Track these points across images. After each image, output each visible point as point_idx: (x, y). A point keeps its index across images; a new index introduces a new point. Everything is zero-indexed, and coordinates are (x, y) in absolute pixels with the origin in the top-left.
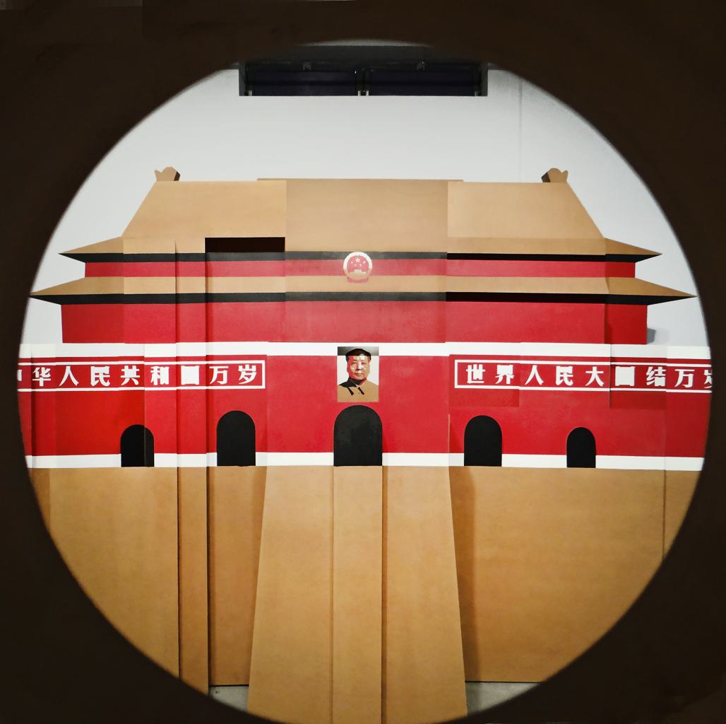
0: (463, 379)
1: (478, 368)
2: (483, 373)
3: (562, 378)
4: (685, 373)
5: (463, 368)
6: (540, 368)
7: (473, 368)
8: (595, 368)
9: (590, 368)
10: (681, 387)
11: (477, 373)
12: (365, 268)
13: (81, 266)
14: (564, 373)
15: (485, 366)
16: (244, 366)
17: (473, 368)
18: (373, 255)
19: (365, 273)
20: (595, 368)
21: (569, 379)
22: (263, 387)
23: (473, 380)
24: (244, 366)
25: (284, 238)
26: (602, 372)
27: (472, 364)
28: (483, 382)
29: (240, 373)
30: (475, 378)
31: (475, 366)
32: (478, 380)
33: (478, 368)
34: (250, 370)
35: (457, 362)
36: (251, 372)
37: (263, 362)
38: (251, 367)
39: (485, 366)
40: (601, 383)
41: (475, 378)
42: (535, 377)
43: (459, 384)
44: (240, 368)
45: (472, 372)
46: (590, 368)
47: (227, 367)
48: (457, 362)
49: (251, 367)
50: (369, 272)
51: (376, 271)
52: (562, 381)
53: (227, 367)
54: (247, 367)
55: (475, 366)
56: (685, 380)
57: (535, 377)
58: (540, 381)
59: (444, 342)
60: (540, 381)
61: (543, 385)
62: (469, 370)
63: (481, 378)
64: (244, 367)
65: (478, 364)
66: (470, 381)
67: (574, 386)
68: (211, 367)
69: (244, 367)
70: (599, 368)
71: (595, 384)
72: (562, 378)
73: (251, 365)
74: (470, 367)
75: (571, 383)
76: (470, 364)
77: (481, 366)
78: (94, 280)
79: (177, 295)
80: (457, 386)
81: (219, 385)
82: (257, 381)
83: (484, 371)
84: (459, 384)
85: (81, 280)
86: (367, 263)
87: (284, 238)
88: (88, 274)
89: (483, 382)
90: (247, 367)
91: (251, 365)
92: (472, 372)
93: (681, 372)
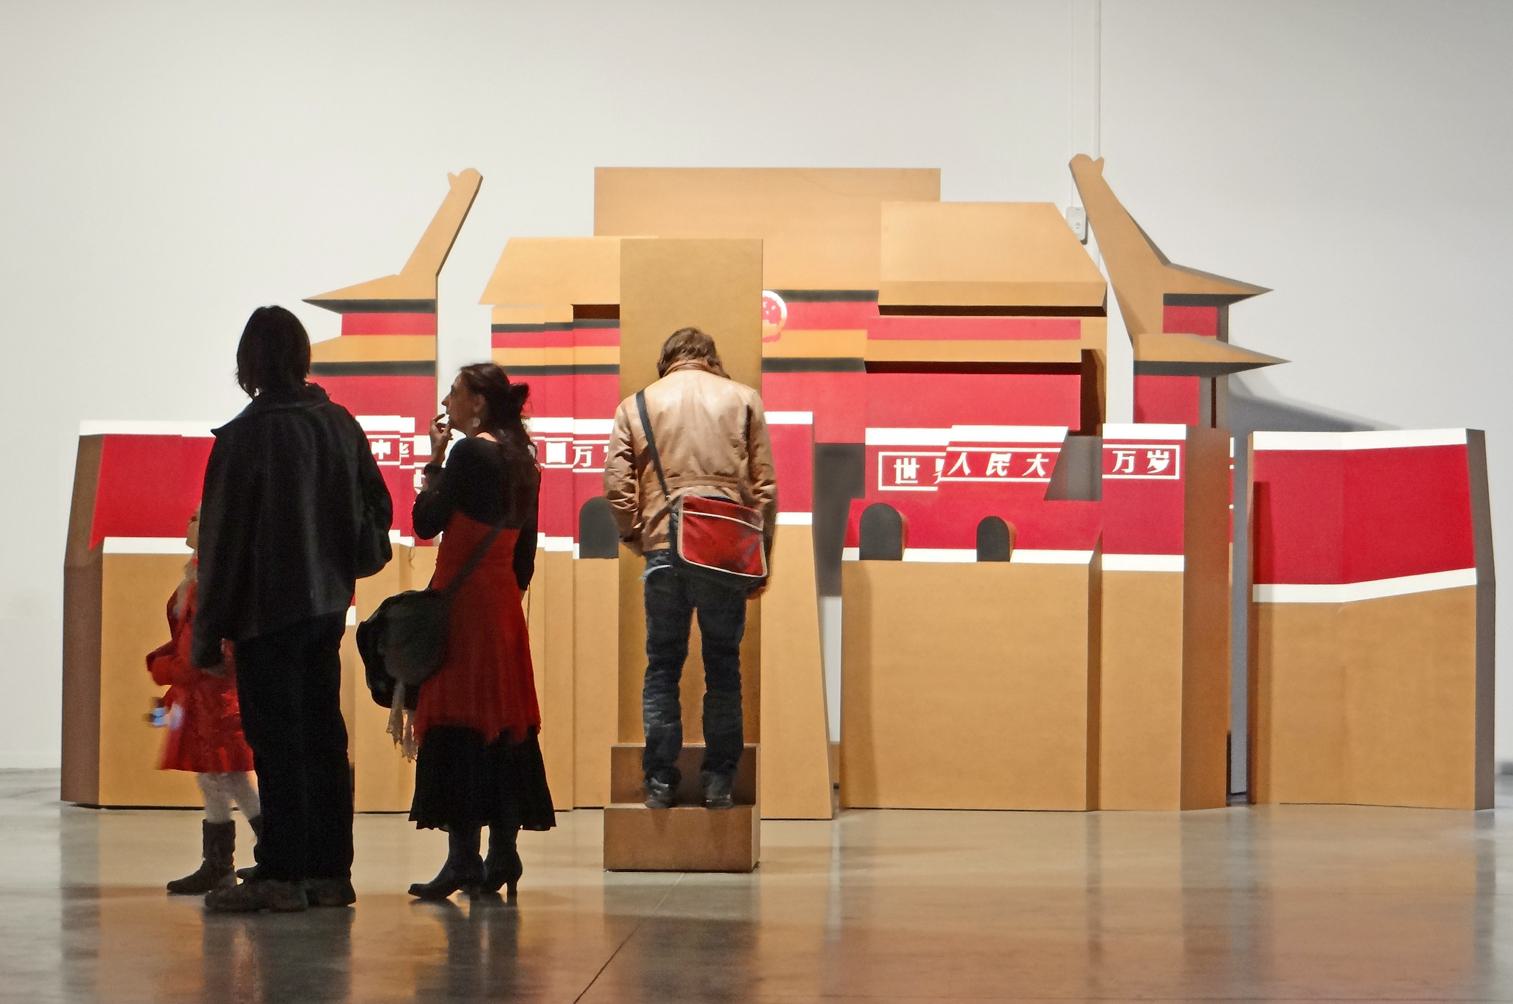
0: (890, 478)
1: (910, 463)
2: (917, 470)
3: (995, 467)
4: (1125, 455)
5: (890, 463)
6: (971, 457)
7: (902, 463)
8: (1039, 456)
9: (1033, 455)
10: (1120, 472)
11: (908, 469)
12: (775, 317)
13: (336, 319)
14: (999, 461)
15: (920, 460)
16: (1154, 451)
17: (902, 463)
18: (788, 295)
19: (775, 325)
20: (1039, 456)
21: (1004, 468)
22: (1177, 477)
23: (903, 479)
24: (1154, 451)
25: (1483, 432)
26: (1047, 460)
27: (902, 458)
28: (916, 482)
29: (1149, 460)
30: (906, 476)
31: (906, 460)
32: (909, 479)
33: (910, 463)
34: (1126, 458)
35: (881, 454)
36: (1162, 459)
37: (1177, 448)
38: (1162, 454)
39: (920, 460)
40: (1041, 472)
41: (906, 476)
42: (961, 467)
43: (884, 484)
44: (1150, 455)
45: (902, 470)
46: (1033, 455)
47: (1134, 452)
48: (881, 454)
49: (1162, 454)
50: (782, 324)
51: (794, 324)
52: (993, 471)
53: (1134, 452)
54: (1158, 453)
55: (906, 460)
56: (1125, 464)
57: (961, 467)
58: (967, 470)
59: (950, 427)
60: (967, 470)
61: (970, 475)
62: (898, 465)
63: (913, 476)
64: (1154, 453)
65: (910, 458)
66: (898, 480)
67: (1008, 476)
68: (1114, 452)
69: (1154, 453)
70: (1045, 455)
71: (1035, 474)
72: (995, 467)
73: (1163, 451)
74: (899, 461)
75: (1005, 473)
76: (1150, 450)
77: (914, 461)
78: (356, 340)
79: (574, 373)
80: (881, 488)
81: (1123, 473)
82: (1170, 470)
83: (918, 466)
84: (884, 484)
85: (335, 340)
86: (778, 309)
87: (1483, 432)
88: (347, 330)
89: (916, 482)
90: (1158, 453)
91: (1163, 451)
92: (902, 470)
93: (1120, 454)
